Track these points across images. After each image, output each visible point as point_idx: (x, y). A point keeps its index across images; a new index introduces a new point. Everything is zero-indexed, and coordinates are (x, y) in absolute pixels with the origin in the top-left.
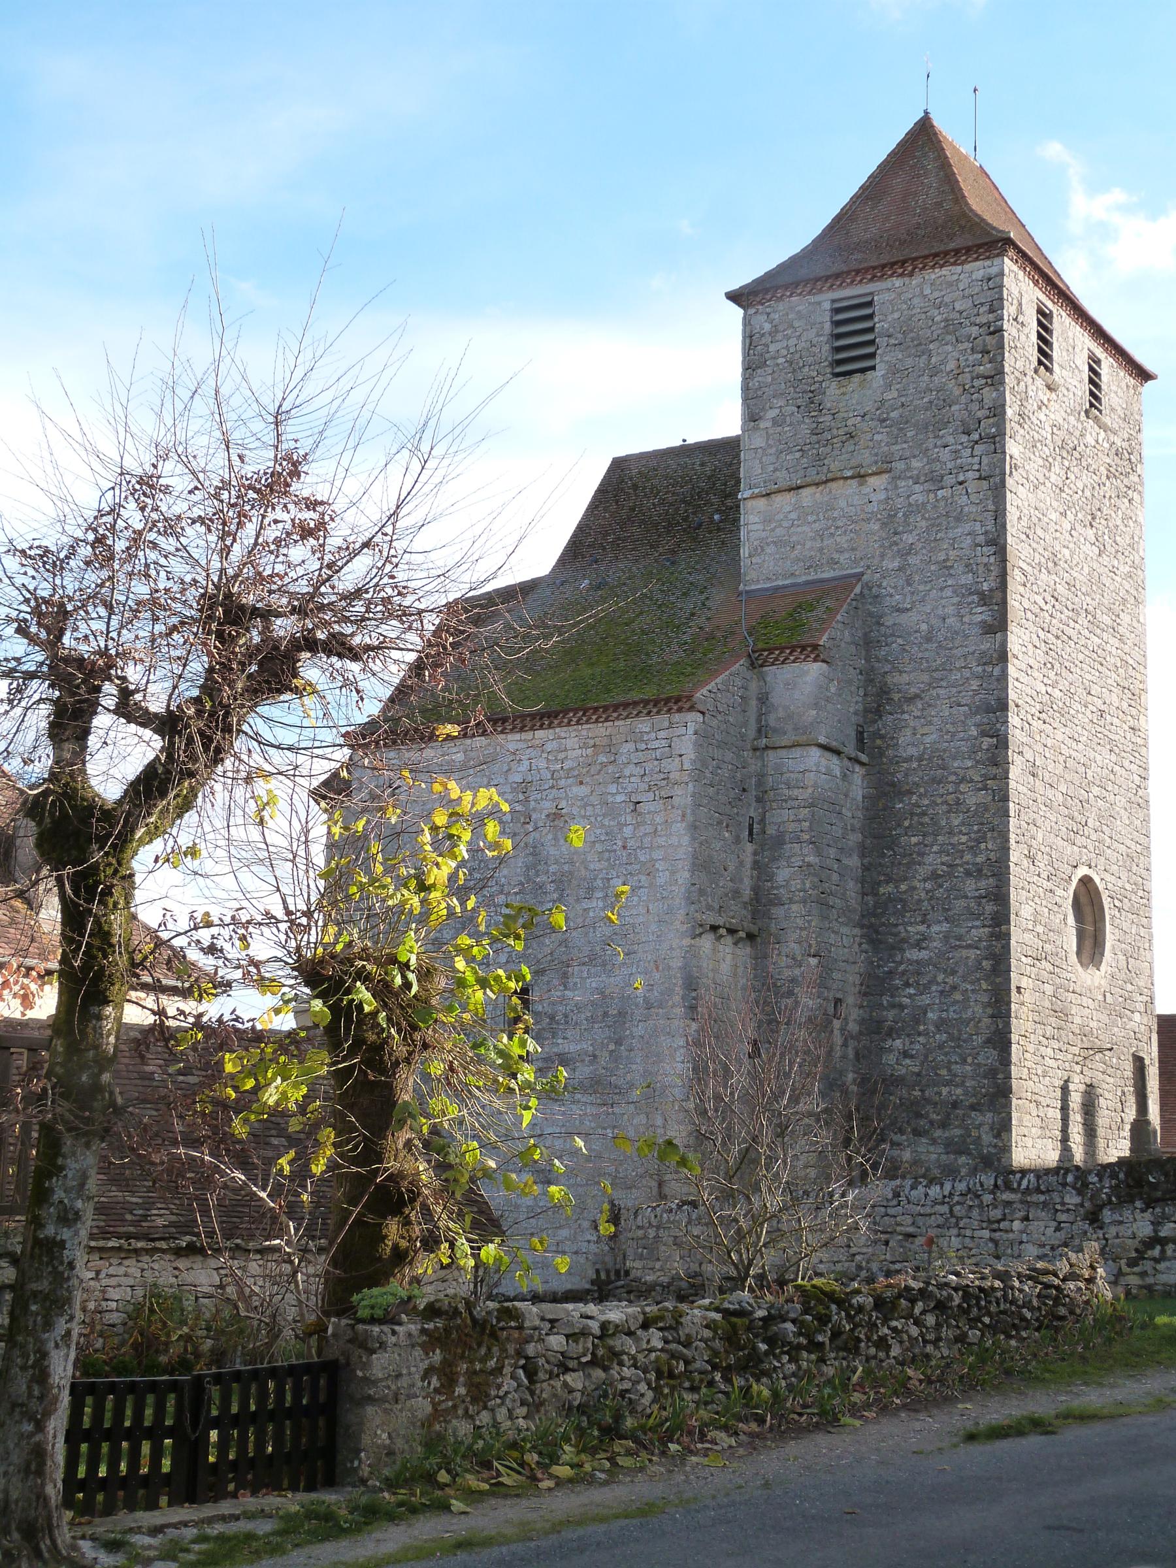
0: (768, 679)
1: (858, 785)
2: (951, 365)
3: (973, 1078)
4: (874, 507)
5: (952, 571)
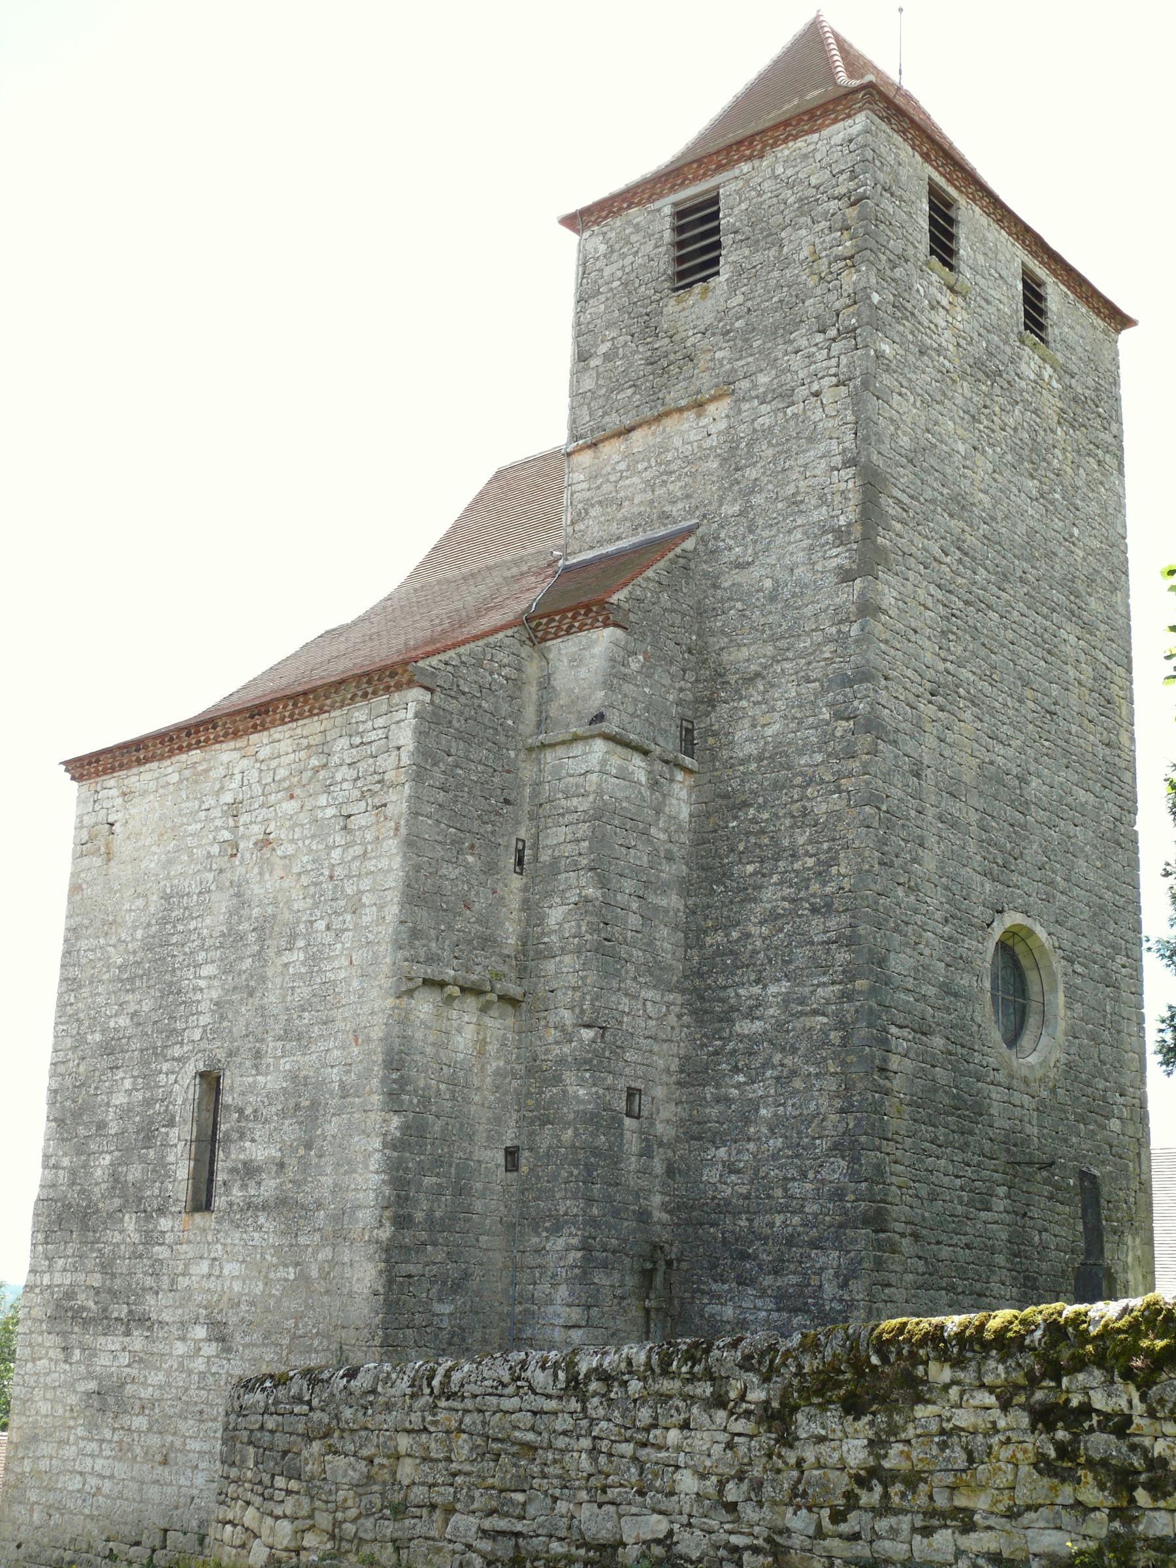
0: (551, 656)
1: (681, 800)
2: (805, 252)
3: (815, 1200)
4: (713, 441)
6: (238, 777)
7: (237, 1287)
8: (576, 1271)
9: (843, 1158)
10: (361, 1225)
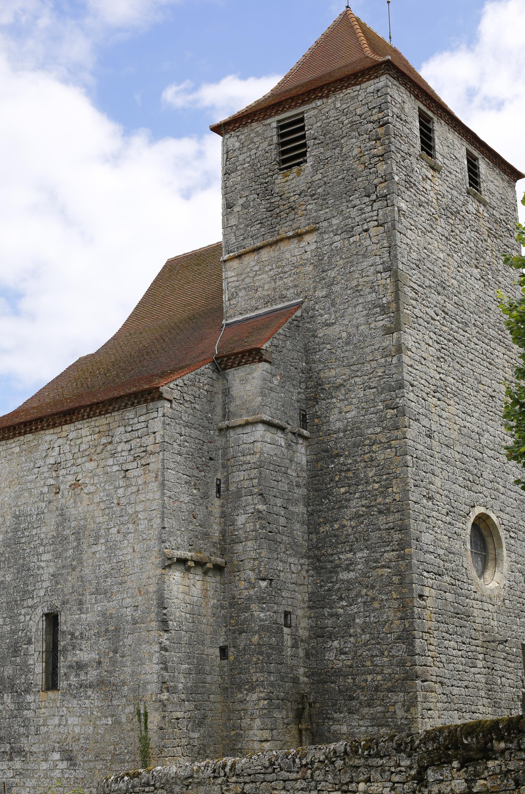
1: (302, 454)
2: (356, 151)
4: (308, 255)
5: (362, 293)
6: (57, 449)
7: (77, 730)
8: (265, 711)
9: (404, 643)
10: (150, 692)
